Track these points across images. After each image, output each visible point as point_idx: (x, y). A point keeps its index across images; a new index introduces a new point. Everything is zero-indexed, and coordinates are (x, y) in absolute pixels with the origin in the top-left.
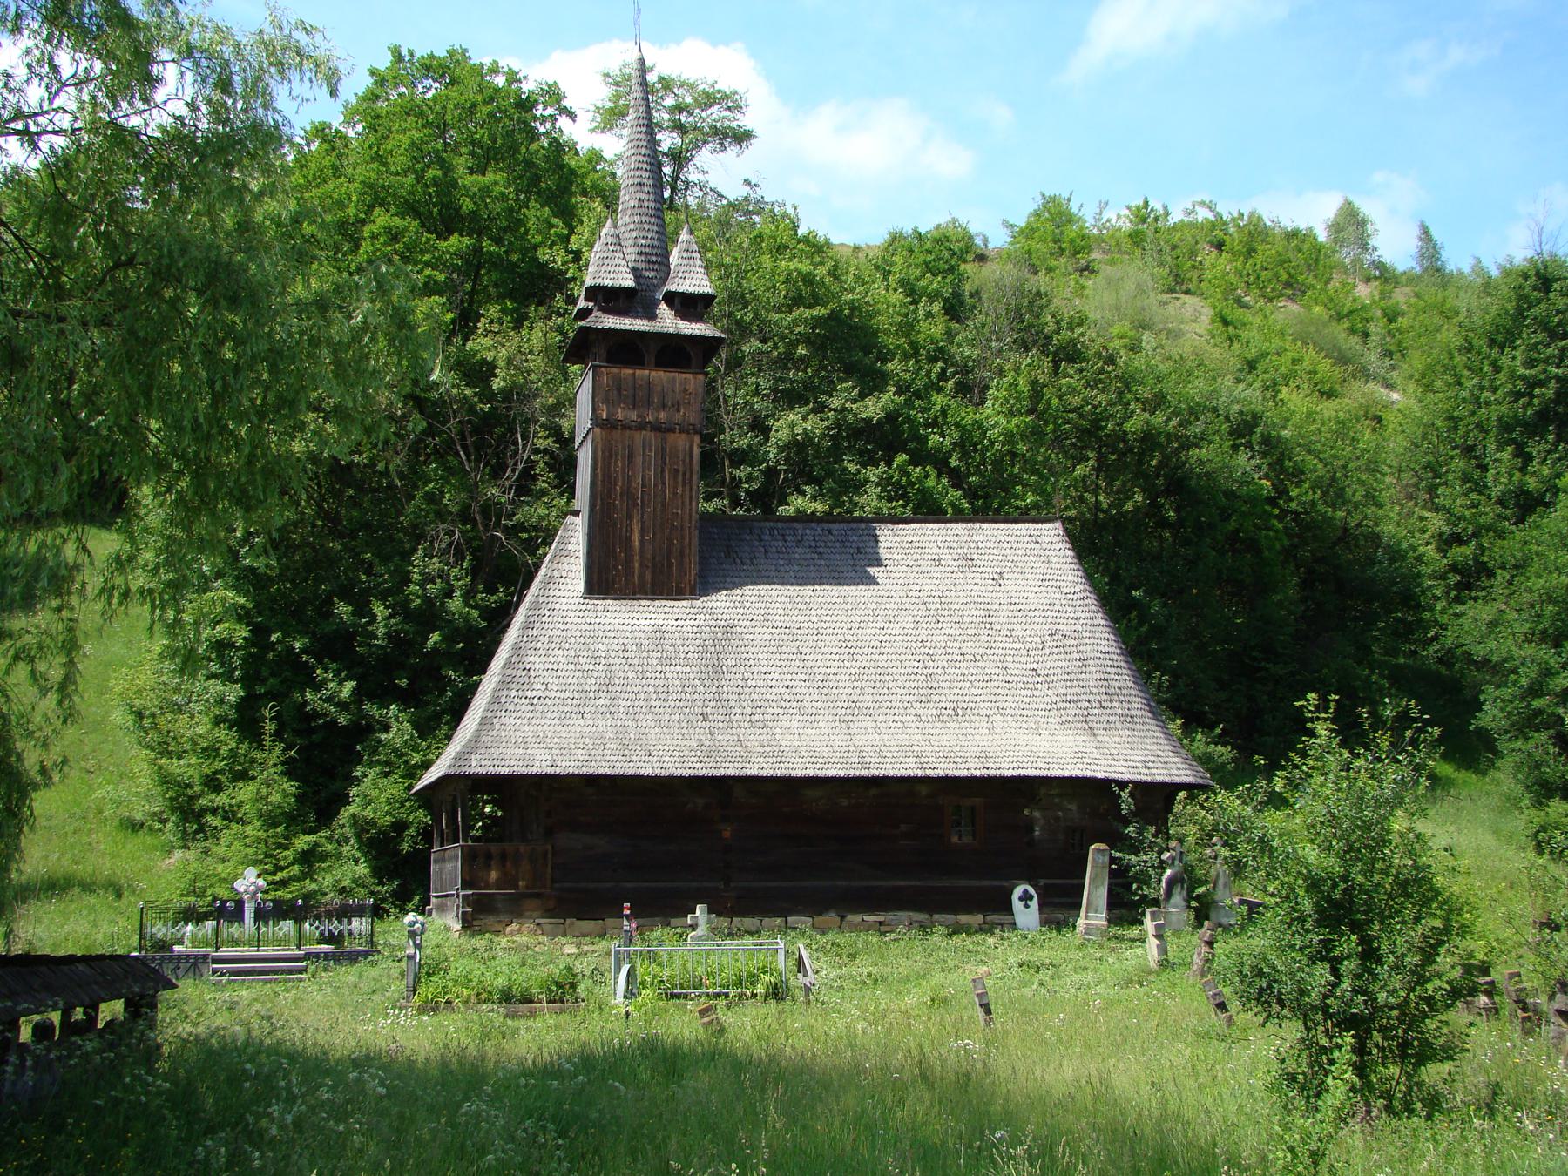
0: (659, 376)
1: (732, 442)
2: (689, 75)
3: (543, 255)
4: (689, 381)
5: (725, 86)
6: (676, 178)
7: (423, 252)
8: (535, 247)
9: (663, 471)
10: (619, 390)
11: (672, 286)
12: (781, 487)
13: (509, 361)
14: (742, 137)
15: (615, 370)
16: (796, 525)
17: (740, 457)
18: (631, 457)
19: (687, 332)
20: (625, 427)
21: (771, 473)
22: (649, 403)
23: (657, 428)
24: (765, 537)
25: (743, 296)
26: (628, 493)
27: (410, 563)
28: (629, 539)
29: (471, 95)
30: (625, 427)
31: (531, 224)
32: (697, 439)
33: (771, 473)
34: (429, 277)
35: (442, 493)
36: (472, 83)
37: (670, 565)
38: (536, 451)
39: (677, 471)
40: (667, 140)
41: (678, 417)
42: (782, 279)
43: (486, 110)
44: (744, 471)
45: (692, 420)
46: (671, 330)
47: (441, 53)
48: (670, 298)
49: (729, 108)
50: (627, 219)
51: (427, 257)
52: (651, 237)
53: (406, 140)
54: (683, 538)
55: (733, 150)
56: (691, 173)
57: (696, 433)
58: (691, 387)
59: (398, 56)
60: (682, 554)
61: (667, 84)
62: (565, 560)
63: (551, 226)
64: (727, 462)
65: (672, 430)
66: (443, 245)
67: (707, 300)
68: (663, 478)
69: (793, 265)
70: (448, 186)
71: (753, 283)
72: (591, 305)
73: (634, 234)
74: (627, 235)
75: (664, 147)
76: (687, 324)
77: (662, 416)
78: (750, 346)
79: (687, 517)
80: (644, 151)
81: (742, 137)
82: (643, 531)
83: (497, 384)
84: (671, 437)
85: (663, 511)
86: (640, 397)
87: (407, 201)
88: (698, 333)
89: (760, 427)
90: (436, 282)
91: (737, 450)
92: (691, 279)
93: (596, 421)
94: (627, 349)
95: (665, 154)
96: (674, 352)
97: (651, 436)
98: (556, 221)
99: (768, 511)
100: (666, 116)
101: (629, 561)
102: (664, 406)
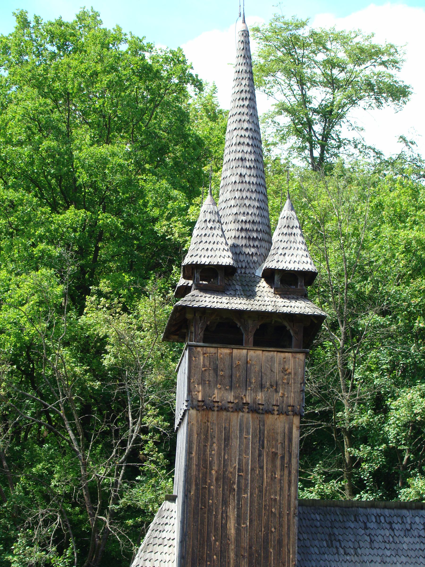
0: (257, 356)
1: (351, 420)
2: (343, 25)
3: (160, 228)
4: (290, 360)
5: (380, 41)
6: (326, 136)
7: (38, 225)
8: (155, 220)
9: (260, 455)
10: (216, 370)
11: (271, 263)
12: (405, 468)
13: (120, 339)
14: (398, 93)
15: (212, 350)
16: (405, 512)
17: (361, 436)
18: (227, 439)
19: (286, 310)
20: (221, 409)
21: (392, 455)
22: (247, 383)
23: (254, 409)
24: (371, 525)
25: (362, 268)
26: (223, 478)
27: (11, 552)
28: (224, 527)
29: (91, 64)
30: (221, 409)
31: (150, 197)
32: (296, 421)
33: (392, 455)
34: (43, 251)
35: (51, 473)
36: (93, 50)
37: (267, 557)
38: (144, 431)
39: (275, 454)
40: (318, 96)
41: (276, 398)
42: (401, 248)
43: (106, 79)
44: (363, 451)
45: (291, 402)
46: (270, 309)
47: (70, 18)
48: (270, 275)
49: (383, 63)
50: (228, 195)
51: (41, 231)
52: (252, 213)
53: (20, 111)
54: (281, 525)
55: (389, 106)
56: (343, 130)
57: (295, 414)
58: (290, 367)
59: (24, 23)
60: (280, 542)
61: (319, 41)
62: (157, 548)
63: (170, 198)
64: (346, 440)
65: (271, 412)
66: (58, 218)
67: (309, 277)
68: (260, 462)
69: (412, 234)
70: (64, 161)
71: (375, 253)
72: (191, 282)
73: (235, 210)
74: (228, 211)
75: (315, 105)
76: (287, 302)
77: (260, 397)
78: (370, 319)
79: (285, 502)
80: (246, 125)
81: (398, 93)
82: (239, 519)
83: (108, 361)
84: (270, 419)
85: (260, 496)
86: (238, 378)
87: (24, 171)
88: (297, 311)
89: (379, 405)
90: (50, 257)
91: (356, 428)
92: (291, 254)
93: (192, 403)
94: (225, 328)
95: (315, 111)
96: (273, 331)
97: (248, 417)
98: (175, 193)
99: (392, 494)
100: (318, 71)
101: (223, 553)
102: (262, 387)
